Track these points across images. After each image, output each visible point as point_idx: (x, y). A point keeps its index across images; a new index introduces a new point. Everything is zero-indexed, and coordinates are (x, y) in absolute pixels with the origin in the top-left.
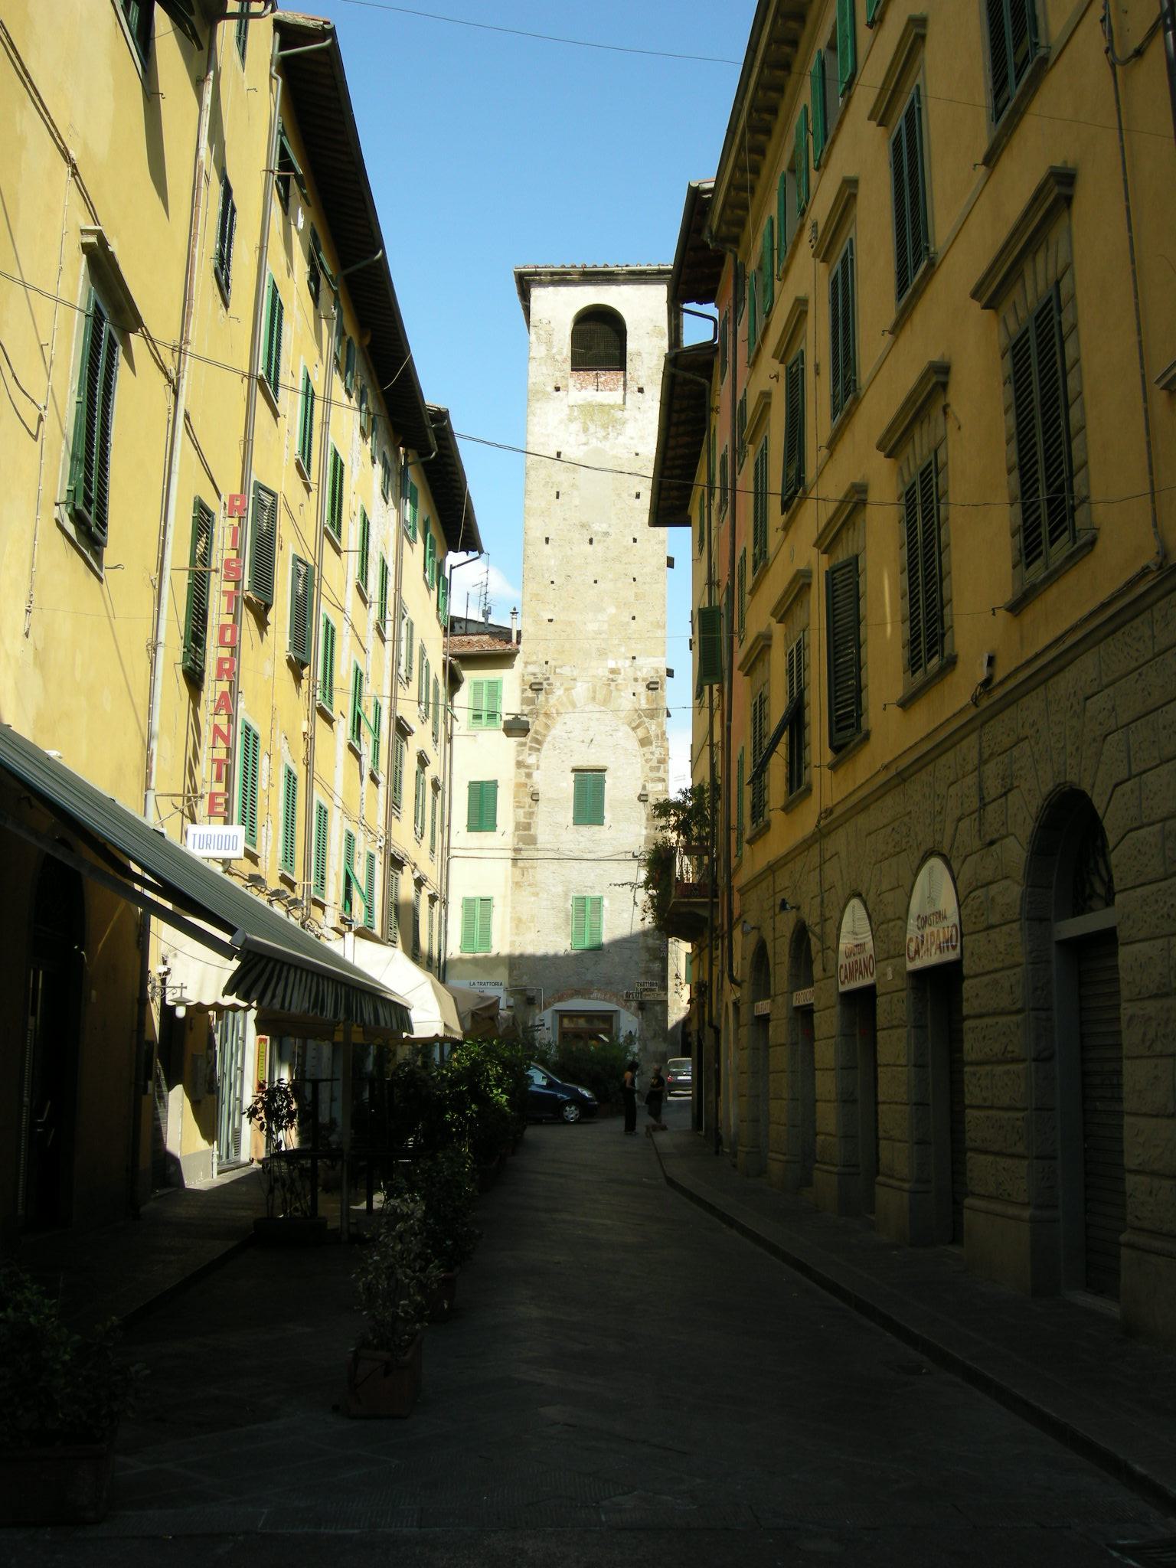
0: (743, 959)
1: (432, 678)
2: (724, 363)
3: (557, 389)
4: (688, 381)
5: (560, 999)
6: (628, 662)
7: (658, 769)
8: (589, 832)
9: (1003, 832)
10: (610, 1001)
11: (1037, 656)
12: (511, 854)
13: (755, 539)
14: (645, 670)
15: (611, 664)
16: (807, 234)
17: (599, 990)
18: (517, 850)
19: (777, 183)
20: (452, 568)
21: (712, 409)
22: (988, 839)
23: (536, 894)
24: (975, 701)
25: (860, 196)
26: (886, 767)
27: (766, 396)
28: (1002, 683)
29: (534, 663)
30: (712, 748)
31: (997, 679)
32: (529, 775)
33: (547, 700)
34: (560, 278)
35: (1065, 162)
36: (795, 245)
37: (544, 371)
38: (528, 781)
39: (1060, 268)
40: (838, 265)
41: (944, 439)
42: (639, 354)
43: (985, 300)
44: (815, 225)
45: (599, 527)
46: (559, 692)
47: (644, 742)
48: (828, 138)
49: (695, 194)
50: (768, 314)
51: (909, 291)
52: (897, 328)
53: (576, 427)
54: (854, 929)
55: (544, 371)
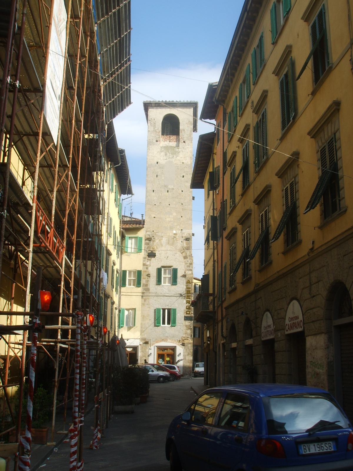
0: (227, 329)
1: (117, 236)
2: (218, 139)
3: (157, 141)
4: (206, 145)
5: (157, 342)
6: (180, 231)
7: (189, 266)
8: (158, 287)
9: (317, 293)
10: (174, 343)
11: (328, 242)
12: (141, 294)
13: (231, 197)
14: (185, 234)
15: (174, 232)
16: (250, 104)
17: (170, 339)
18: (143, 293)
19: (239, 86)
20: (123, 200)
21: (213, 153)
22: (312, 295)
23: (149, 308)
24: (308, 254)
25: (268, 96)
26: (278, 272)
27: (234, 154)
28: (317, 249)
29: (149, 231)
30: (214, 260)
31: (315, 248)
32: (147, 268)
33: (153, 243)
34: (158, 105)
35: (337, 99)
36: (246, 107)
37: (153, 135)
38: (147, 270)
39: (336, 129)
40: (261, 116)
41: (297, 175)
42: (184, 130)
43: (312, 136)
44: (253, 102)
45: (170, 187)
46: (157, 241)
47: (185, 257)
48: (257, 77)
49: (211, 87)
50: (235, 127)
51: (286, 128)
52: (282, 139)
53: (163, 154)
54: (268, 320)
55: (153, 135)
